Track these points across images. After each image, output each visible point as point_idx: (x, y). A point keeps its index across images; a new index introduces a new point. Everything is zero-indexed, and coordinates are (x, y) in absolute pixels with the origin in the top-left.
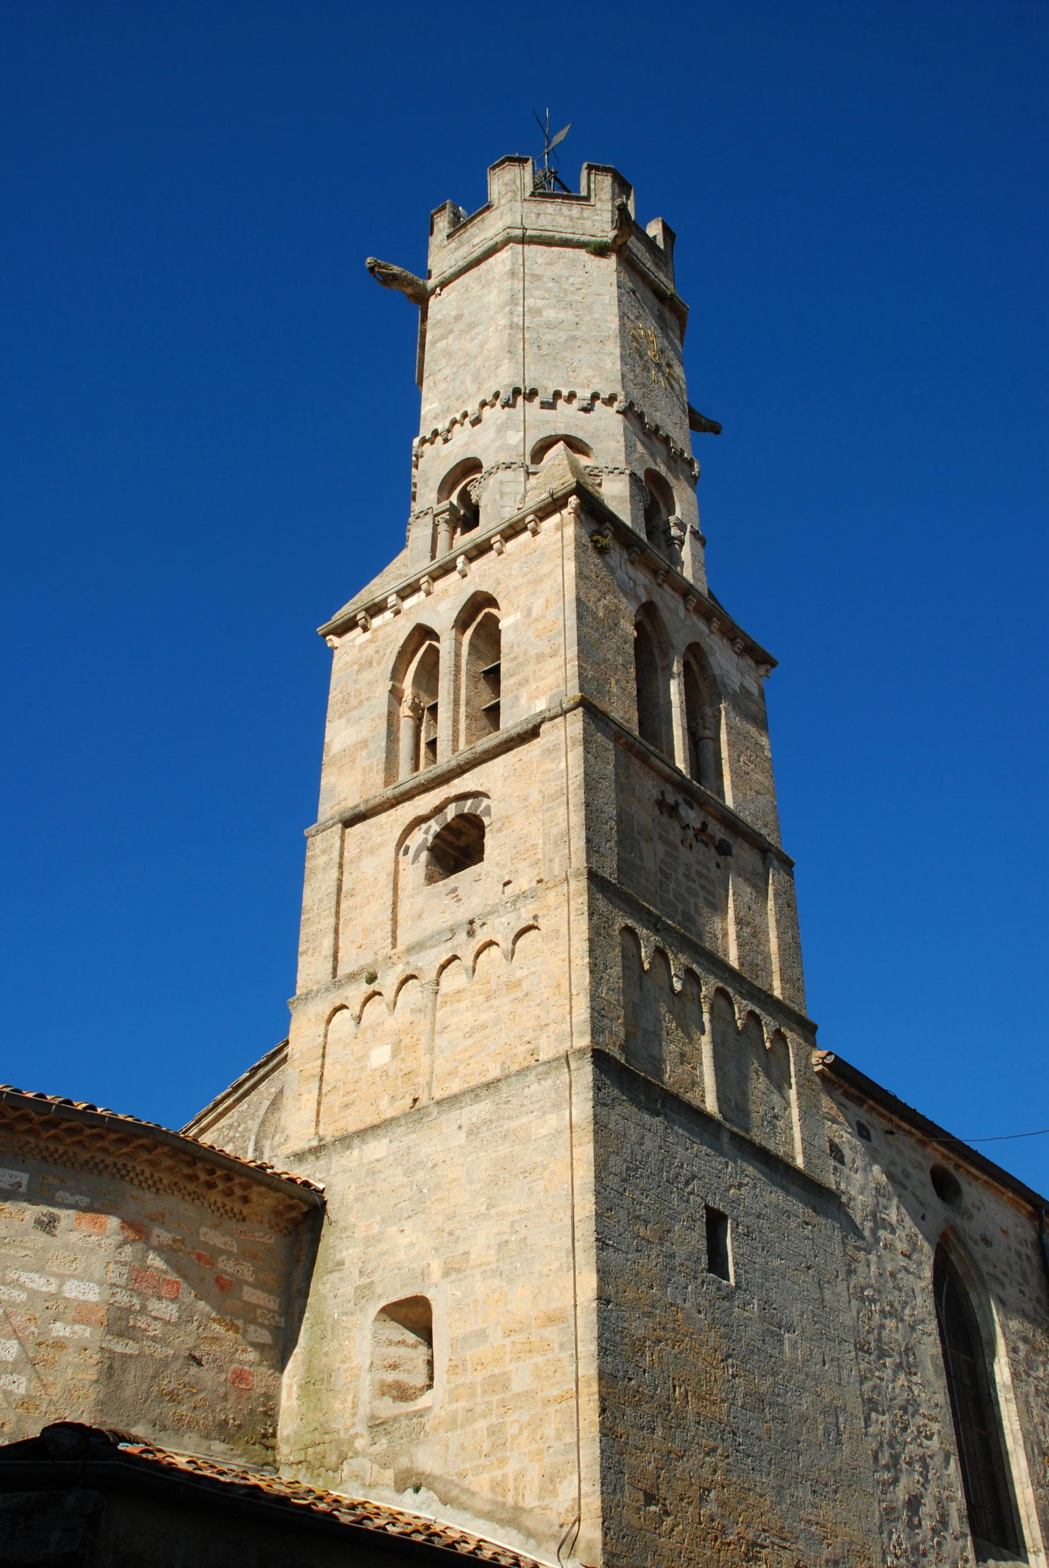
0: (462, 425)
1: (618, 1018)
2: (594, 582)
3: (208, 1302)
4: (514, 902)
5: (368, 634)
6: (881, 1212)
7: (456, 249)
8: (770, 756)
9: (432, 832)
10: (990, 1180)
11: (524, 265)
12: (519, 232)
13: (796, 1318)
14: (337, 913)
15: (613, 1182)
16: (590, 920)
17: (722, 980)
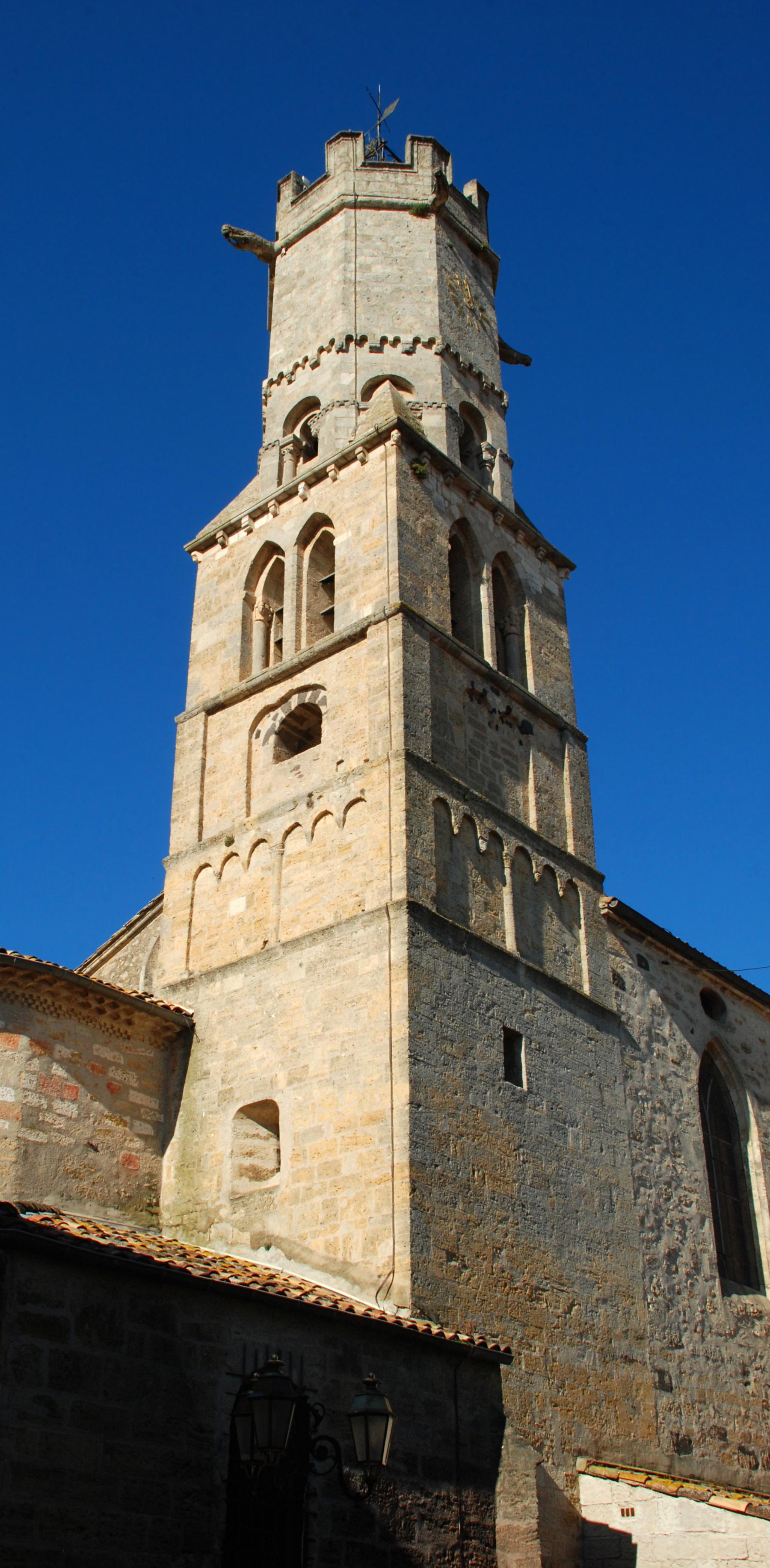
0: (304, 368)
1: (431, 875)
2: (413, 504)
3: (101, 1101)
4: (345, 779)
5: (226, 550)
6: (655, 1028)
7: (299, 214)
8: (568, 647)
9: (279, 718)
10: (751, 999)
11: (356, 227)
12: (351, 199)
13: (579, 1115)
14: (202, 787)
15: (424, 1009)
16: (407, 793)
17: (521, 839)
